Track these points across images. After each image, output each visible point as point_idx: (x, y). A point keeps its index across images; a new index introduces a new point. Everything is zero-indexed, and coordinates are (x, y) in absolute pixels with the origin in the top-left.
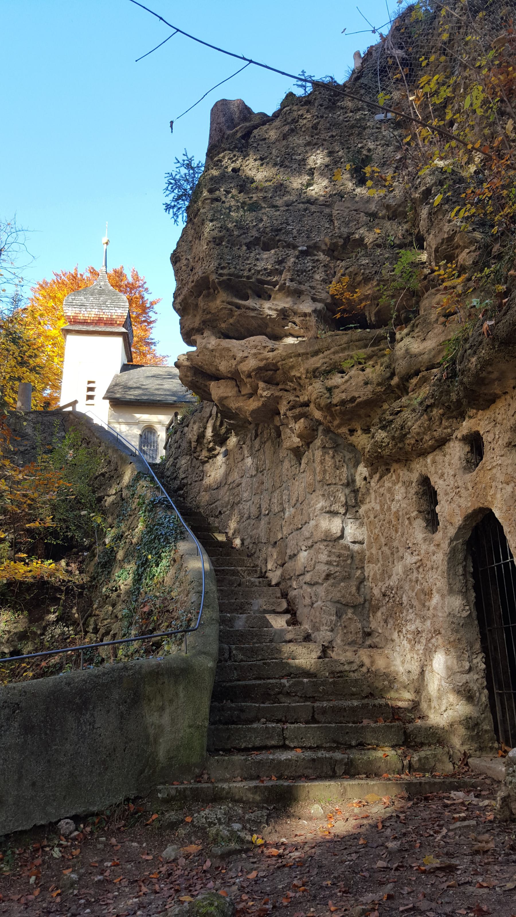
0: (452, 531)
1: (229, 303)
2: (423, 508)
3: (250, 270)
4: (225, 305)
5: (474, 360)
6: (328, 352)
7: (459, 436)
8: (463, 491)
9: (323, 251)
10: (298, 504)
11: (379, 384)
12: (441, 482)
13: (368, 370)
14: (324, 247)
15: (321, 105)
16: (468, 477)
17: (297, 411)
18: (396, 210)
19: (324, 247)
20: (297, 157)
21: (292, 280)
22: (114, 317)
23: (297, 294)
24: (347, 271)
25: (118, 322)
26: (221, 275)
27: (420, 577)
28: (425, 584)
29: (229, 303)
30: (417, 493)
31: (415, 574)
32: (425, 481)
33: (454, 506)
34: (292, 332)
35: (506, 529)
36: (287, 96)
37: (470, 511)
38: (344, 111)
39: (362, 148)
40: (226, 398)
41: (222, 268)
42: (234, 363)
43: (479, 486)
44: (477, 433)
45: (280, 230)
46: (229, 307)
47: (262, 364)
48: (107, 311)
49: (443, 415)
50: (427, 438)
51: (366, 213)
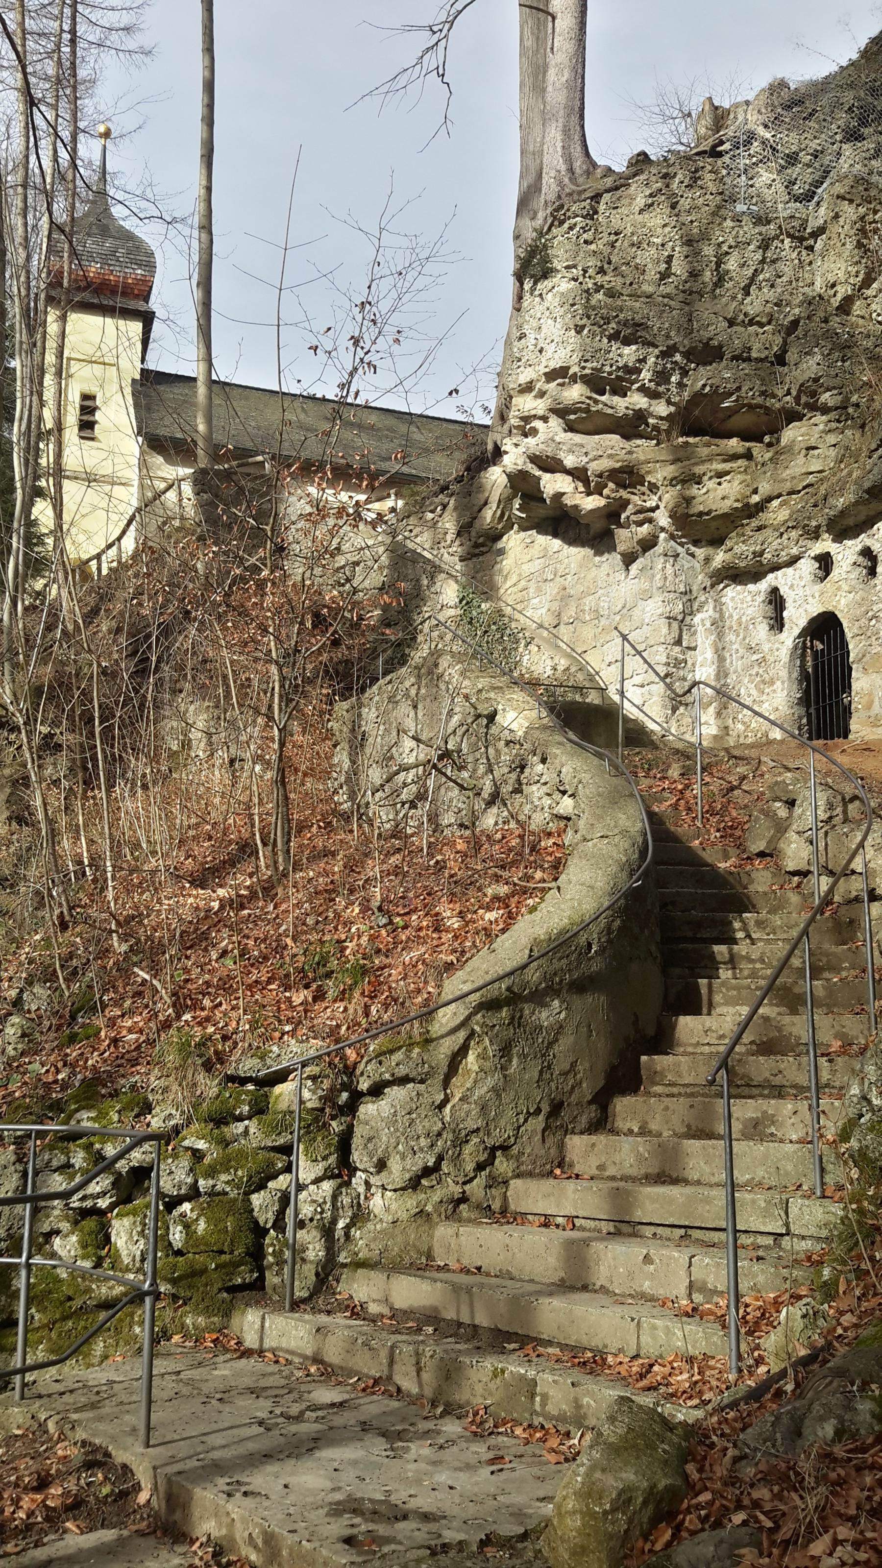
0: (797, 631)
1: (589, 398)
2: (769, 614)
3: (611, 366)
4: (583, 399)
5: (842, 500)
6: (688, 462)
7: (812, 555)
8: (810, 599)
9: (681, 353)
10: (625, 611)
11: (737, 501)
12: (790, 592)
13: (725, 485)
14: (681, 349)
15: (682, 182)
16: (819, 587)
17: (641, 516)
18: (753, 318)
19: (681, 349)
20: (655, 240)
21: (650, 381)
22: (130, 281)
23: (654, 395)
24: (709, 382)
25: (136, 292)
26: (584, 368)
27: (761, 671)
28: (766, 675)
29: (589, 398)
30: (764, 601)
31: (756, 669)
32: (775, 591)
33: (801, 610)
34: (643, 433)
35: (845, 625)
36: (639, 155)
37: (815, 614)
38: (704, 191)
39: (723, 242)
40: (564, 494)
41: (586, 361)
42: (586, 460)
43: (825, 595)
44: (828, 554)
45: (642, 324)
46: (588, 401)
47: (618, 465)
48: (117, 268)
49: (801, 536)
50: (783, 553)
51: (725, 318)
